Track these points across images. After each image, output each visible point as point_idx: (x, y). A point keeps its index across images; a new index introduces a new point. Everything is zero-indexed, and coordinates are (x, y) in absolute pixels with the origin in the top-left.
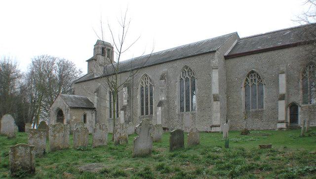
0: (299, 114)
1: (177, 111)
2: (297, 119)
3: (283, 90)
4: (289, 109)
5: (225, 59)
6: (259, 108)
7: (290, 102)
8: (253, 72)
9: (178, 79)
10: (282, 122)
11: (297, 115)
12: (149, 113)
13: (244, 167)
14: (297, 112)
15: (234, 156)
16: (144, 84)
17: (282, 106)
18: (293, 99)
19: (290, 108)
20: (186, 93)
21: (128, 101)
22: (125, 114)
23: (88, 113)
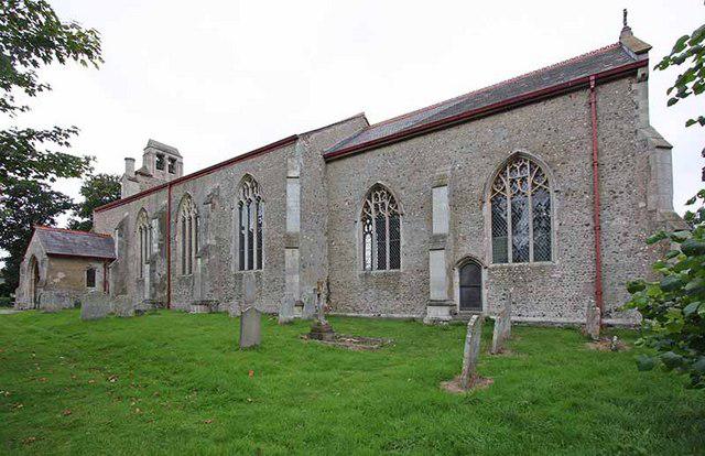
0: (483, 287)
1: (234, 269)
2: (480, 298)
3: (441, 225)
4: (457, 272)
5: (327, 162)
6: (535, 260)
7: (460, 256)
8: (378, 187)
9: (236, 202)
10: (440, 304)
11: (480, 287)
12: (246, 267)
13: (231, 442)
14: (480, 282)
15: (215, 402)
16: (373, 211)
17: (438, 264)
18: (467, 250)
19: (461, 272)
20: (390, 224)
21: (160, 246)
22: (152, 271)
23: (99, 267)
